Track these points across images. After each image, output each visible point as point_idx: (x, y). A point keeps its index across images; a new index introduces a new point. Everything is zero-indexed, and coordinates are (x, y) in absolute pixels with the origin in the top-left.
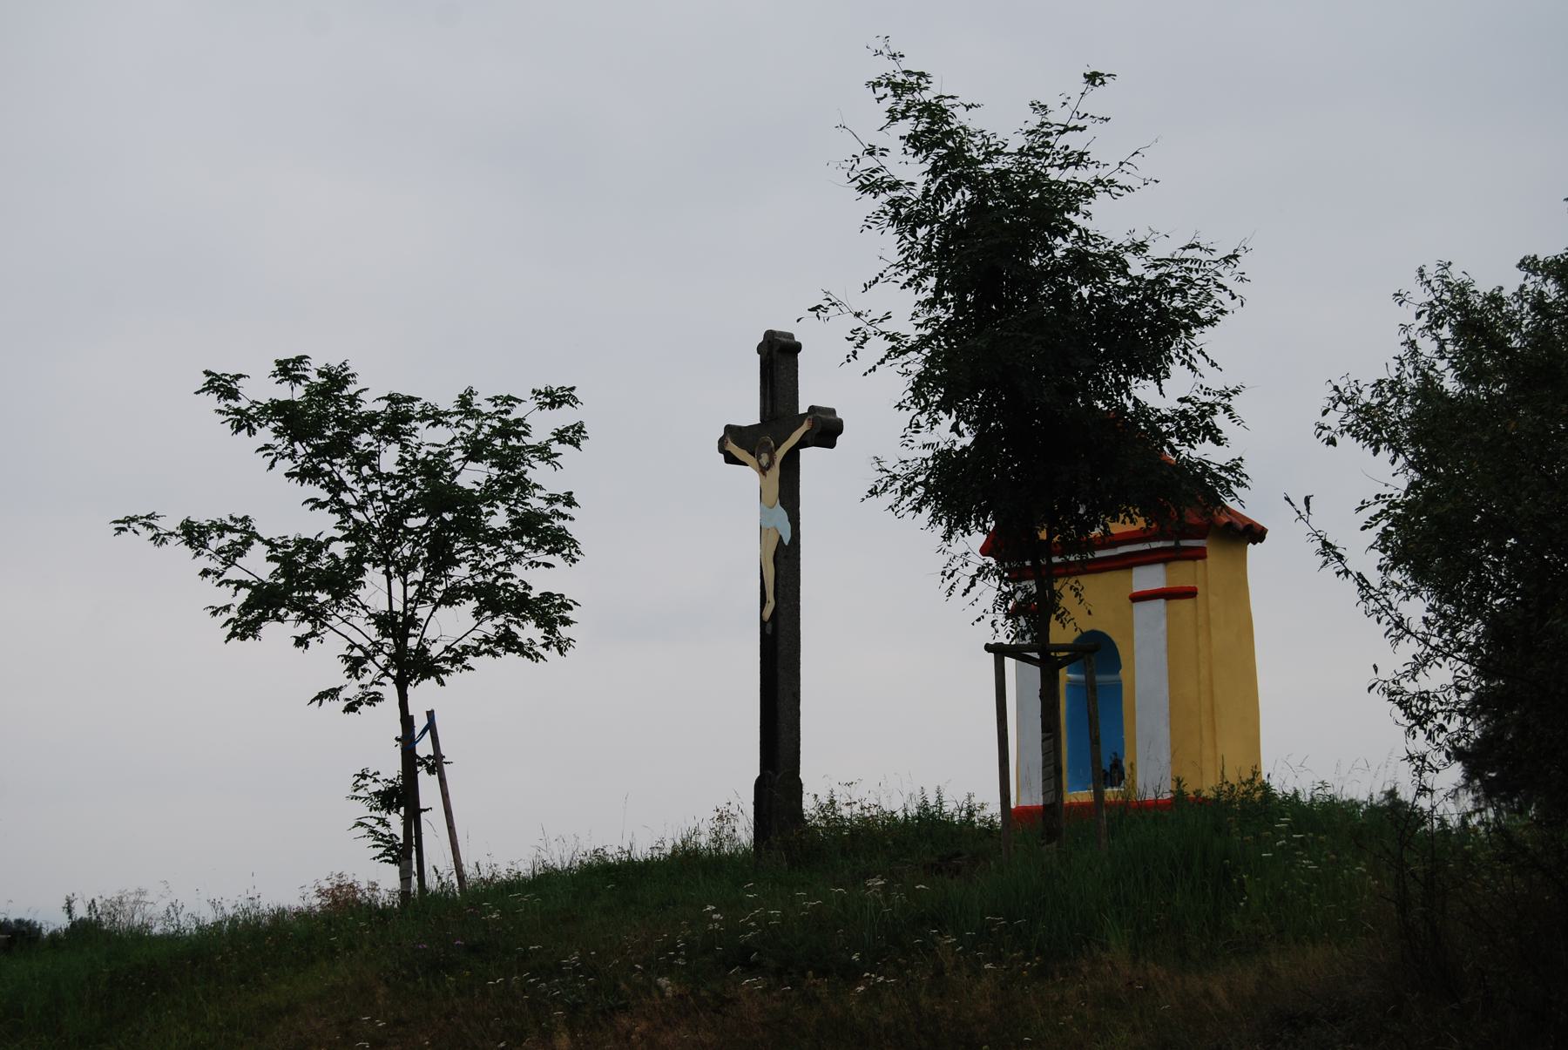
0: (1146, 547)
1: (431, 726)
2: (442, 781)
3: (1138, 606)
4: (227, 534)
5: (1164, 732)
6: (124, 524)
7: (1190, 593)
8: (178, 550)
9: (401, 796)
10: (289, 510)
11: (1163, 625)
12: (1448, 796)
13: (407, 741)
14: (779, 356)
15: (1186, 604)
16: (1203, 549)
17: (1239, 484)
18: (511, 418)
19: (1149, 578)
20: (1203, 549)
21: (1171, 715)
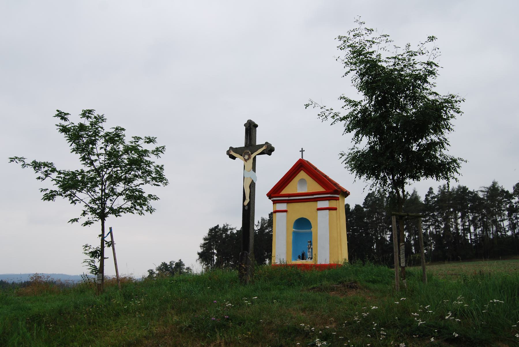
0: (287, 198)
1: (111, 232)
2: (114, 249)
3: (319, 212)
4: (46, 167)
5: (328, 246)
6: (12, 160)
7: (335, 209)
8: (31, 169)
9: (98, 254)
10: (71, 162)
11: (328, 217)
12: (197, 267)
13: (102, 236)
14: (251, 128)
15: (335, 211)
17: (459, 167)
18: (138, 144)
19: (325, 204)
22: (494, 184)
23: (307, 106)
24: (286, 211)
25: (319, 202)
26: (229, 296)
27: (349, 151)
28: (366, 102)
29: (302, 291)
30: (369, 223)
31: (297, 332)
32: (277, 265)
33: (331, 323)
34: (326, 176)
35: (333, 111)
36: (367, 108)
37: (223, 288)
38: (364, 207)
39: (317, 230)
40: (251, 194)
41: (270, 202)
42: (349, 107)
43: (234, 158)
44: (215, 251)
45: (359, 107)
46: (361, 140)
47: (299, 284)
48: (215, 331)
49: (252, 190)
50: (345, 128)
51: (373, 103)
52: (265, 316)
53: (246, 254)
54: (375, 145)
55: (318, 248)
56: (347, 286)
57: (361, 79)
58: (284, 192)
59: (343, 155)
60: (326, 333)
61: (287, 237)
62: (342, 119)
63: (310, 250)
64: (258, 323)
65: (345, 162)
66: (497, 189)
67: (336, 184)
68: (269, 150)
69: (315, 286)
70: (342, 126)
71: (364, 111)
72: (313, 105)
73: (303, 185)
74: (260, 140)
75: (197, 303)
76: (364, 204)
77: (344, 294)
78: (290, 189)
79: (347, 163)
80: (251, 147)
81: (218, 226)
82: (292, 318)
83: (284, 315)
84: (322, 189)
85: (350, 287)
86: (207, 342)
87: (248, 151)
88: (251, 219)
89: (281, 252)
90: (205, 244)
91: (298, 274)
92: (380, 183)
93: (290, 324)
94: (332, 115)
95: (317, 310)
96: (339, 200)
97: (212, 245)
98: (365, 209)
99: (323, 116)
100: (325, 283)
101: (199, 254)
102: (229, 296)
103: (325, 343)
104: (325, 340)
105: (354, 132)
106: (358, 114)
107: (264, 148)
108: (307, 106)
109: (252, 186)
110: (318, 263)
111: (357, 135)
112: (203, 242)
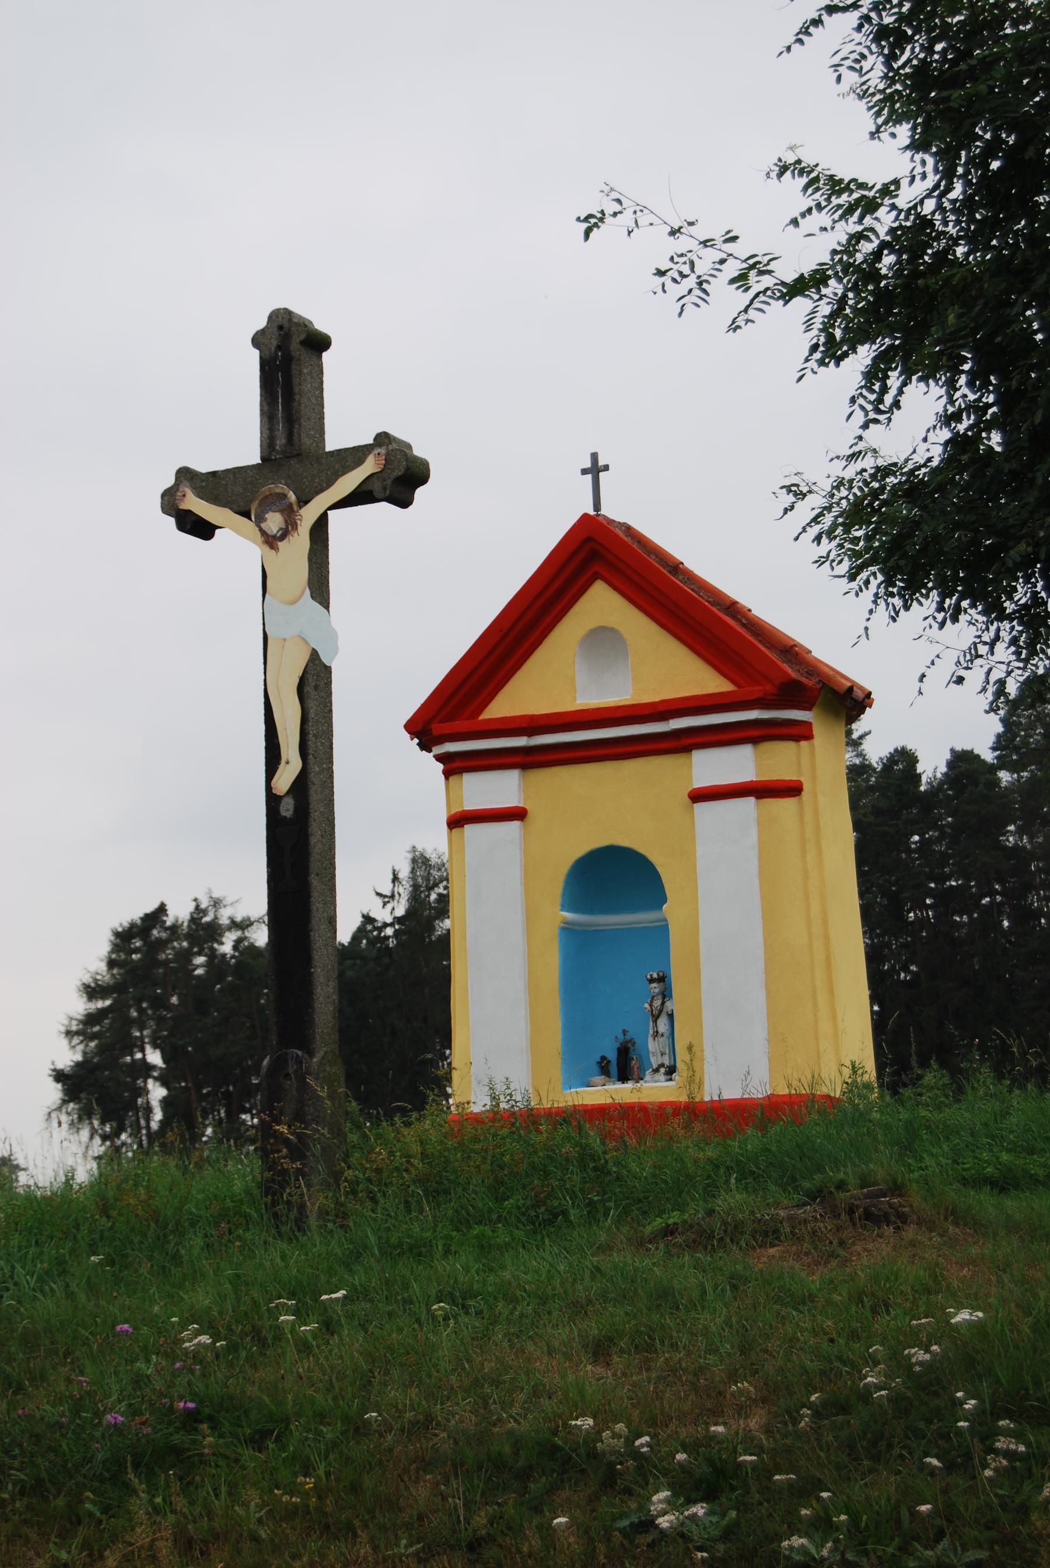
3: (701, 808)
5: (756, 997)
7: (791, 790)
14: (290, 355)
16: (808, 725)
19: (735, 764)
20: (808, 725)
21: (767, 972)
22: (952, 750)
23: (591, 223)
24: (517, 814)
25: (699, 757)
26: (202, 1298)
27: (838, 470)
28: (921, 187)
29: (607, 1248)
30: (1032, 856)
31: (559, 1463)
32: (477, 1119)
33: (742, 1411)
34: (733, 608)
35: (741, 249)
36: (925, 223)
37: (176, 1258)
38: (1003, 763)
40: (312, 730)
41: (429, 766)
42: (823, 218)
43: (203, 530)
44: (154, 1057)
45: (884, 221)
46: (896, 404)
47: (593, 1213)
48: (127, 1485)
49: (311, 704)
50: (805, 342)
51: (957, 191)
52: (393, 1393)
53: (299, 1061)
54: (982, 426)
55: (705, 1014)
56: (851, 1211)
57: (890, 59)
58: (505, 705)
59: (801, 495)
60: (710, 1461)
62: (797, 288)
63: (663, 1025)
64: (359, 1429)
65: (815, 530)
67: (791, 652)
68: (399, 477)
69: (674, 1218)
70: (793, 325)
71: (914, 234)
72: (626, 219)
74: (343, 427)
75: (29, 1341)
76: (1001, 743)
77: (832, 1255)
78: (534, 690)
79: (830, 533)
80: (295, 465)
81: (162, 909)
82: (536, 1393)
83: (496, 1383)
85: (868, 1216)
86: (86, 1545)
87: (281, 488)
88: (314, 866)
89: (503, 1044)
90: (90, 1019)
91: (586, 1157)
92: (1014, 641)
93: (525, 1426)
94: (733, 268)
95: (674, 1346)
96: (809, 737)
97: (132, 1022)
98: (1005, 777)
99: (683, 277)
100: (733, 1200)
101: (59, 1076)
102: (202, 1298)
103: (699, 1510)
104: (709, 1495)
105: (865, 355)
106: (877, 255)
107: (369, 467)
108: (591, 223)
109: (315, 683)
110: (709, 1093)
111: (875, 375)
112: (80, 1006)
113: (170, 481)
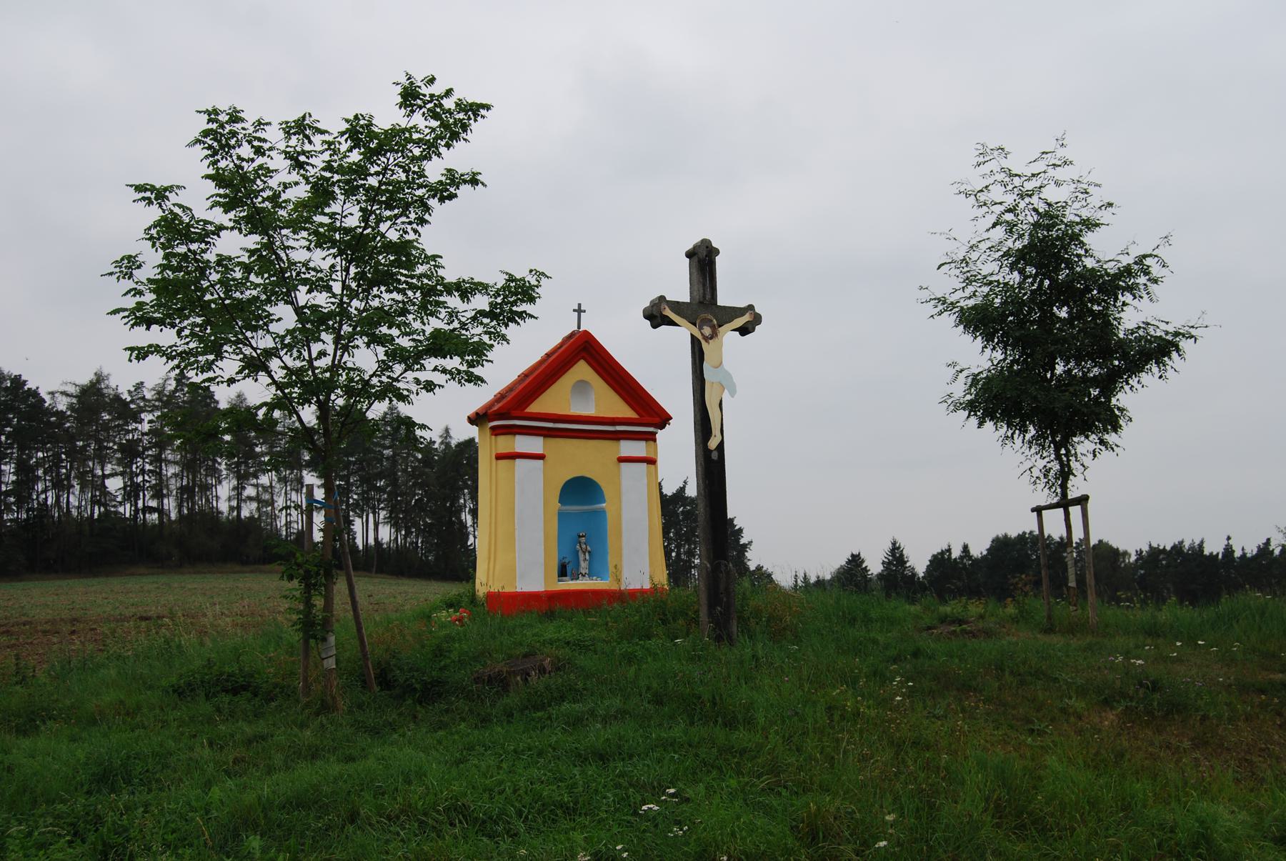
3: (623, 465)
11: (645, 481)
14: (703, 260)
22: (100, 378)
23: (921, 288)
24: (540, 457)
39: (620, 509)
58: (535, 408)
61: (545, 522)
66: (99, 393)
73: (581, 396)
84: (629, 413)
87: (710, 317)
108: (921, 288)
113: (757, 310)
